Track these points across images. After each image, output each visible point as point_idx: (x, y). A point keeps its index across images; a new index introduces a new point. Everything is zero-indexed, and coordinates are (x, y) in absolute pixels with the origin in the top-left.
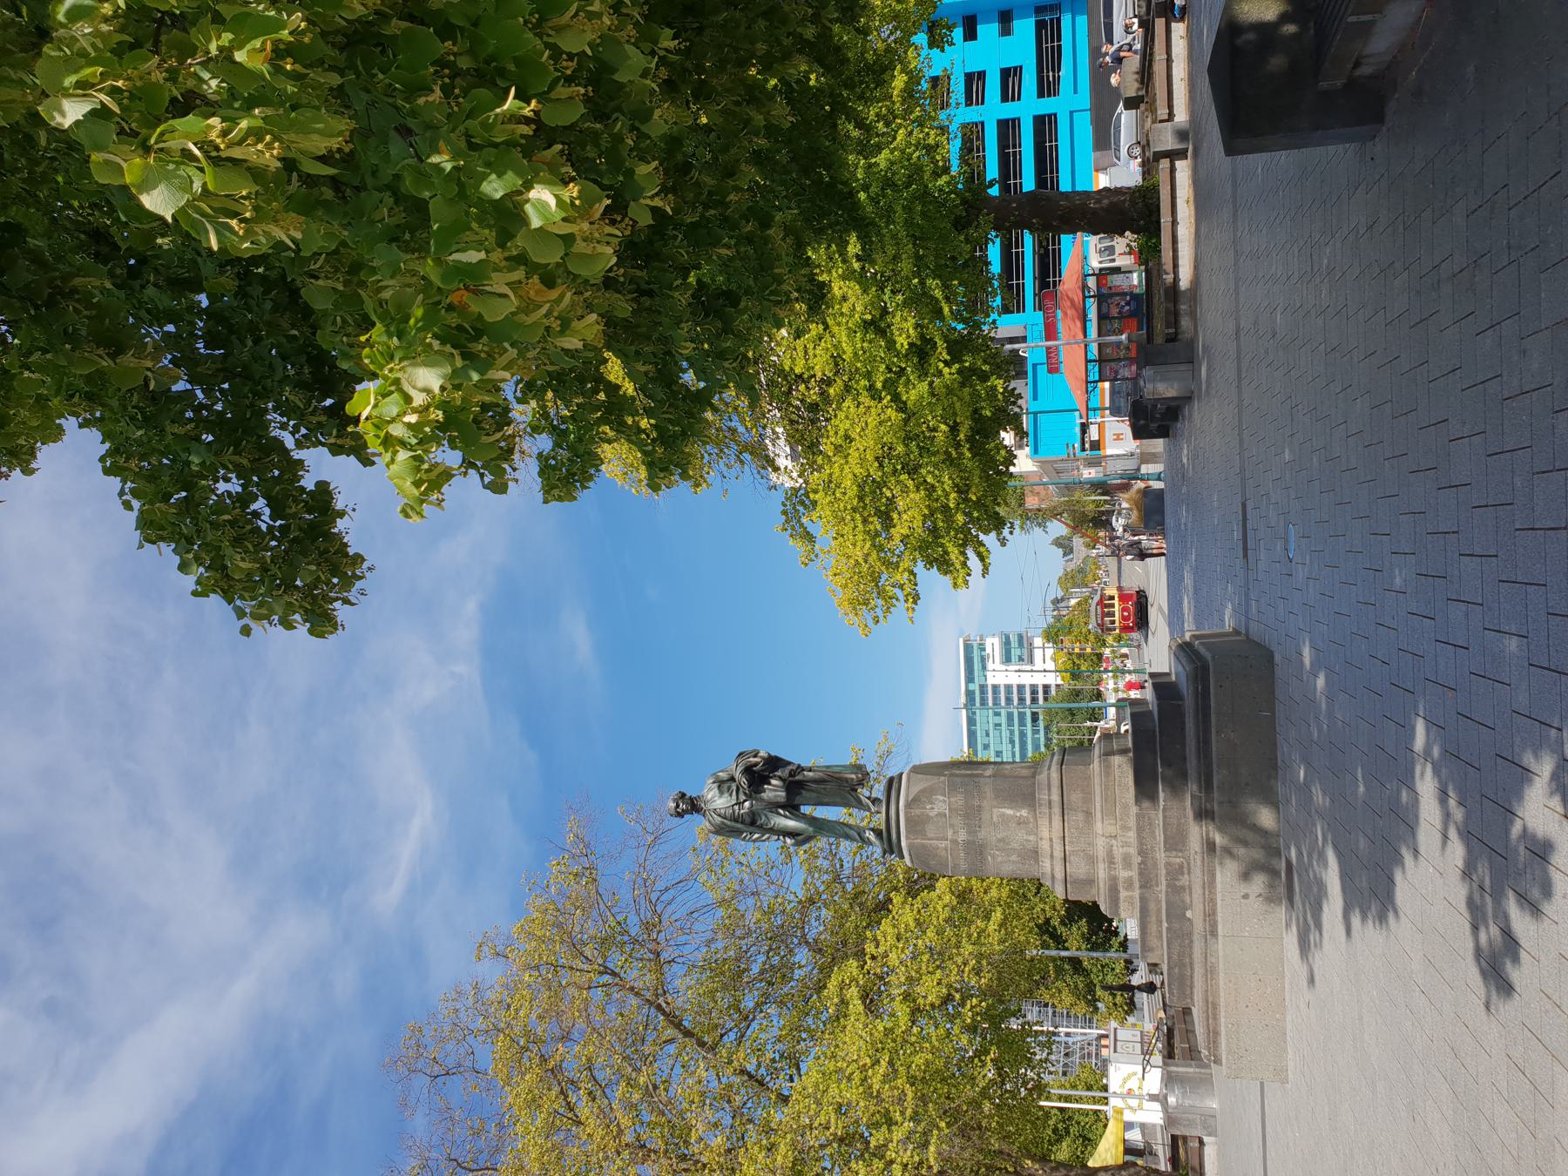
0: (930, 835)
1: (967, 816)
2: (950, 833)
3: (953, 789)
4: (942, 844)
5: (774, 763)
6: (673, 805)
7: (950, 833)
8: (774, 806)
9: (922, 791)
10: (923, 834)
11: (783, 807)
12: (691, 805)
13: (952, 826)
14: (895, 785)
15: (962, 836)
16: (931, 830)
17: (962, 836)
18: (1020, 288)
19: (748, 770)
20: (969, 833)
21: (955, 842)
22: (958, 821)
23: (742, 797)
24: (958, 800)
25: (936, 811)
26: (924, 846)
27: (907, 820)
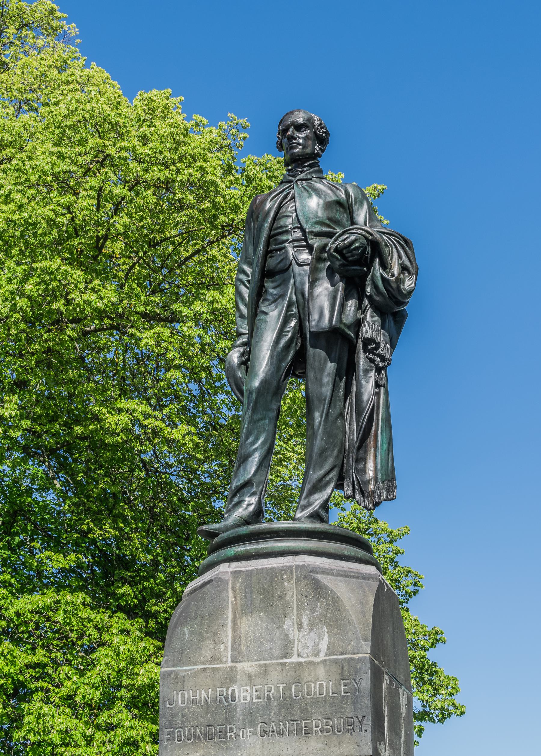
0: (245, 623)
1: (287, 703)
2: (247, 667)
3: (345, 671)
4: (226, 648)
5: (392, 309)
6: (300, 119)
7: (247, 667)
8: (302, 307)
9: (336, 604)
10: (247, 608)
11: (300, 329)
12: (303, 155)
13: (265, 671)
14: (361, 553)
15: (244, 694)
16: (252, 625)
17: (244, 694)
18: (206, 664)
19: (374, 250)
20: (251, 712)
21: (231, 677)
22: (275, 684)
23: (316, 243)
24: (321, 683)
25: (295, 635)
26: (216, 614)
27: (272, 573)
